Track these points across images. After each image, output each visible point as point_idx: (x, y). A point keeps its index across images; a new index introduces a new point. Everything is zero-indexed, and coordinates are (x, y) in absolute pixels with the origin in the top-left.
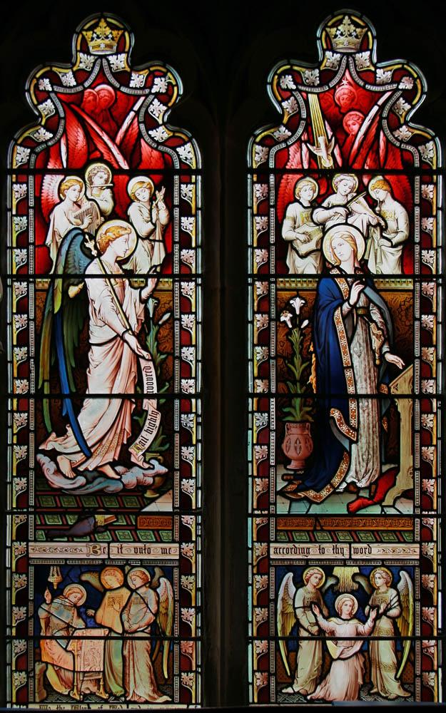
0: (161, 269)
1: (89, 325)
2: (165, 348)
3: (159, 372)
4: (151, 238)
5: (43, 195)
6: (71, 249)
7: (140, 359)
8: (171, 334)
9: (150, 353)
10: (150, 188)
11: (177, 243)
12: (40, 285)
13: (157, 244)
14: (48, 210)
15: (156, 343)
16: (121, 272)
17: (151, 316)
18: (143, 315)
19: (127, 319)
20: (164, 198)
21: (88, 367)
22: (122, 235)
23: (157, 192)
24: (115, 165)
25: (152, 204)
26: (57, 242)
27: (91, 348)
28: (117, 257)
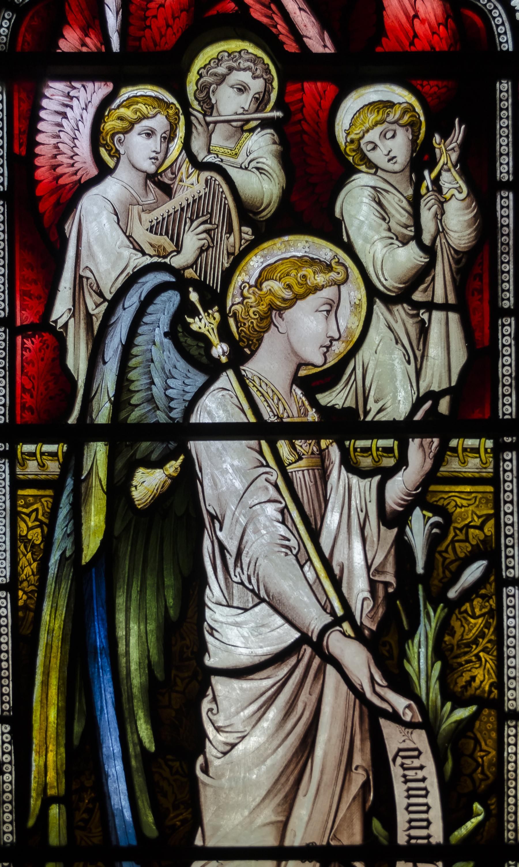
0: (452, 405)
1: (202, 606)
2: (469, 683)
3: (449, 765)
4: (418, 296)
5: (38, 150)
6: (139, 340)
7: (382, 722)
8: (490, 634)
9: (416, 699)
10: (414, 125)
11: (508, 313)
12: (32, 466)
13: (437, 316)
14: (57, 203)
15: (438, 665)
16: (312, 416)
17: (420, 569)
18: (390, 568)
19: (337, 583)
20: (460, 160)
21: (202, 750)
22: (317, 289)
23: (437, 138)
24: (291, 47)
25: (421, 179)
26: (89, 317)
27: (209, 684)
28: (299, 366)
